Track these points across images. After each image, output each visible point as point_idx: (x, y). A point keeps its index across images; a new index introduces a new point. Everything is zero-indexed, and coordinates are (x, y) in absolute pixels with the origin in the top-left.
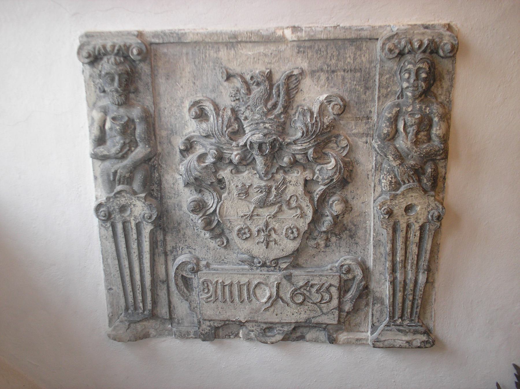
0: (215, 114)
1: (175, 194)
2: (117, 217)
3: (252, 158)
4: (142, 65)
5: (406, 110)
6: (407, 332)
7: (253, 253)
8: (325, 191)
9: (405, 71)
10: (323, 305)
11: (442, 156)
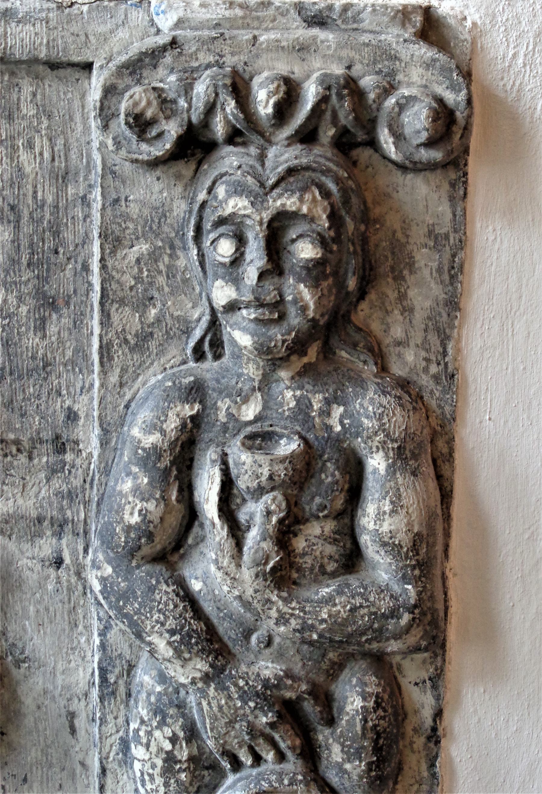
5: (230, 415)
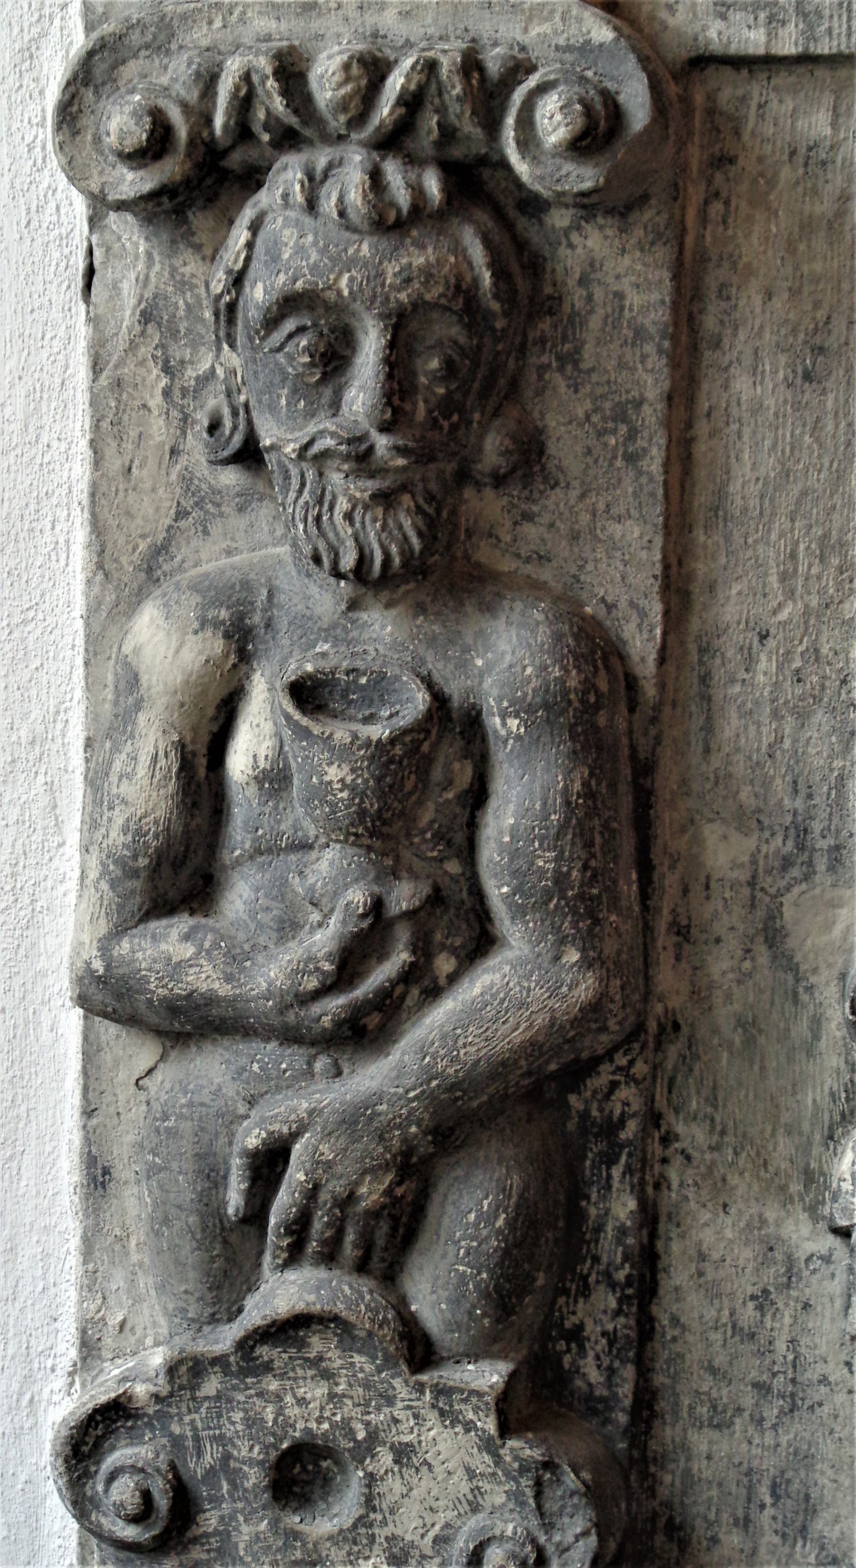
2: (244, 1533)
4: (595, 241)
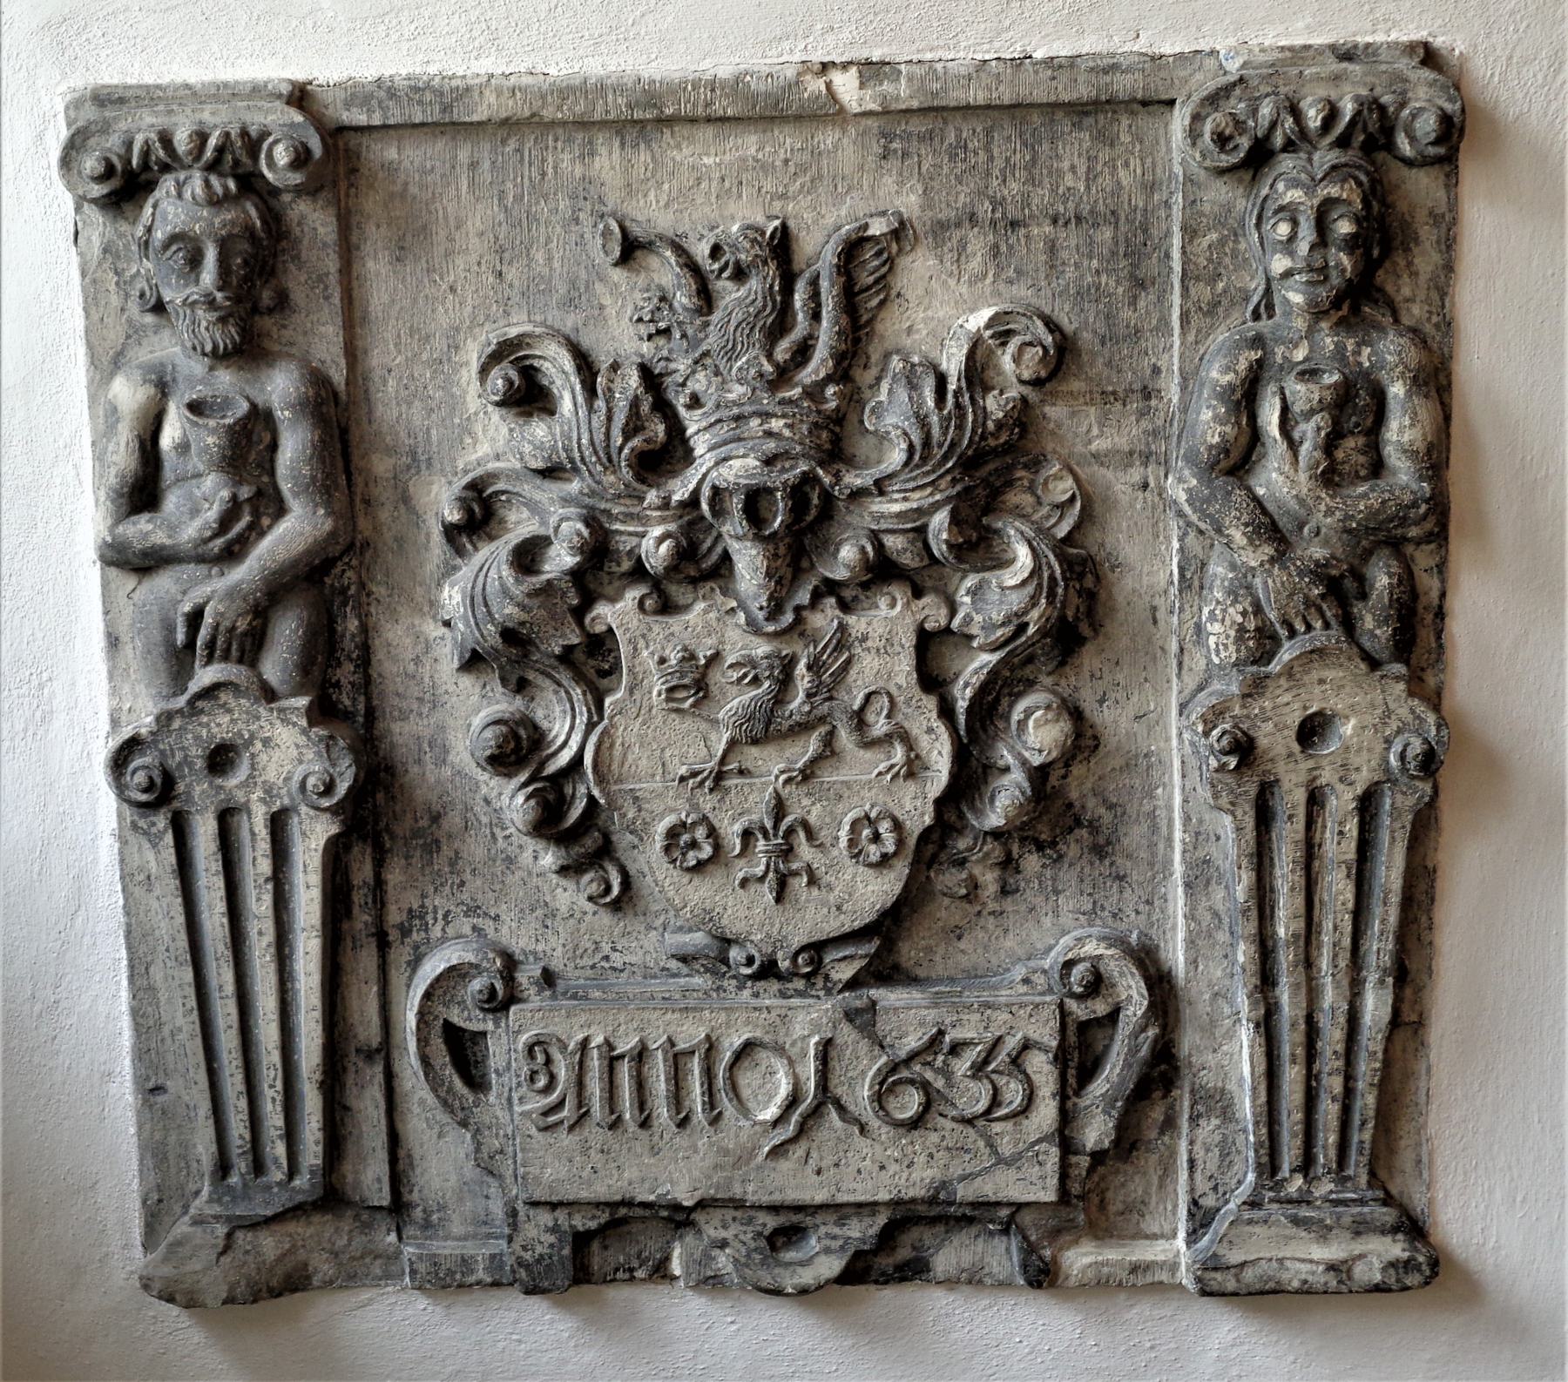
0: (578, 387)
1: (420, 700)
3: (719, 549)
5: (1285, 358)
6: (1330, 1228)
7: (725, 922)
8: (994, 673)
9: (1276, 212)
10: (997, 1127)
11: (1429, 525)
